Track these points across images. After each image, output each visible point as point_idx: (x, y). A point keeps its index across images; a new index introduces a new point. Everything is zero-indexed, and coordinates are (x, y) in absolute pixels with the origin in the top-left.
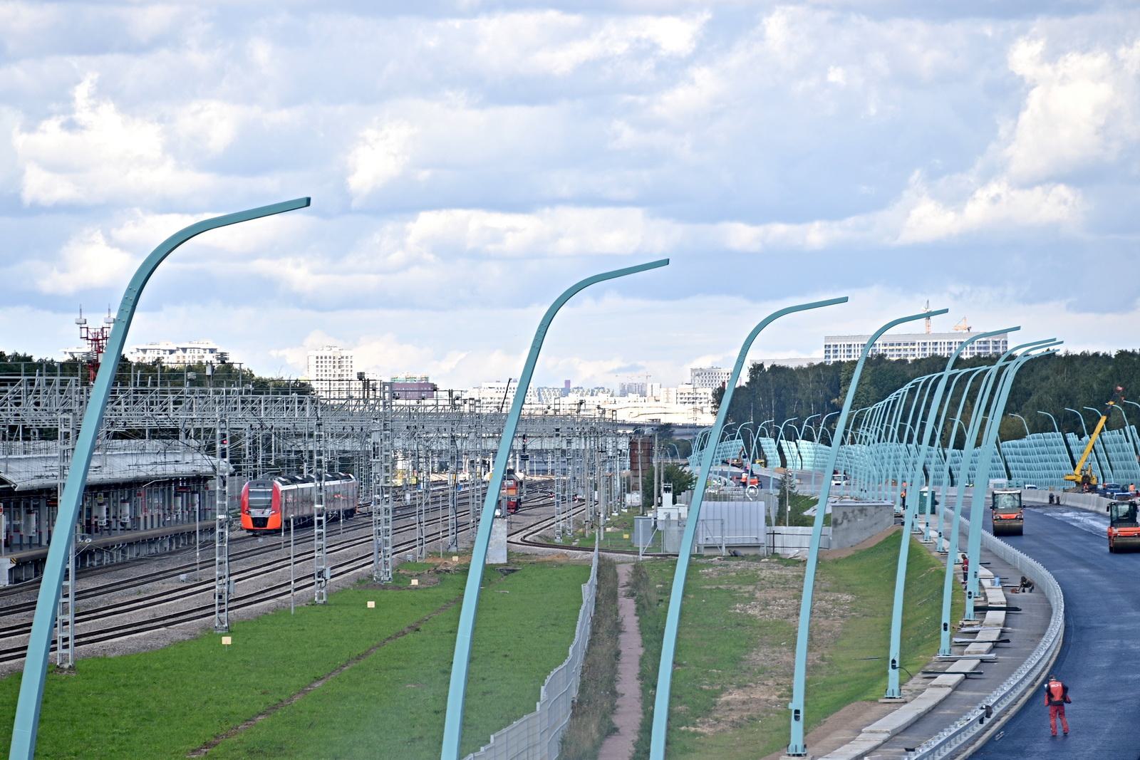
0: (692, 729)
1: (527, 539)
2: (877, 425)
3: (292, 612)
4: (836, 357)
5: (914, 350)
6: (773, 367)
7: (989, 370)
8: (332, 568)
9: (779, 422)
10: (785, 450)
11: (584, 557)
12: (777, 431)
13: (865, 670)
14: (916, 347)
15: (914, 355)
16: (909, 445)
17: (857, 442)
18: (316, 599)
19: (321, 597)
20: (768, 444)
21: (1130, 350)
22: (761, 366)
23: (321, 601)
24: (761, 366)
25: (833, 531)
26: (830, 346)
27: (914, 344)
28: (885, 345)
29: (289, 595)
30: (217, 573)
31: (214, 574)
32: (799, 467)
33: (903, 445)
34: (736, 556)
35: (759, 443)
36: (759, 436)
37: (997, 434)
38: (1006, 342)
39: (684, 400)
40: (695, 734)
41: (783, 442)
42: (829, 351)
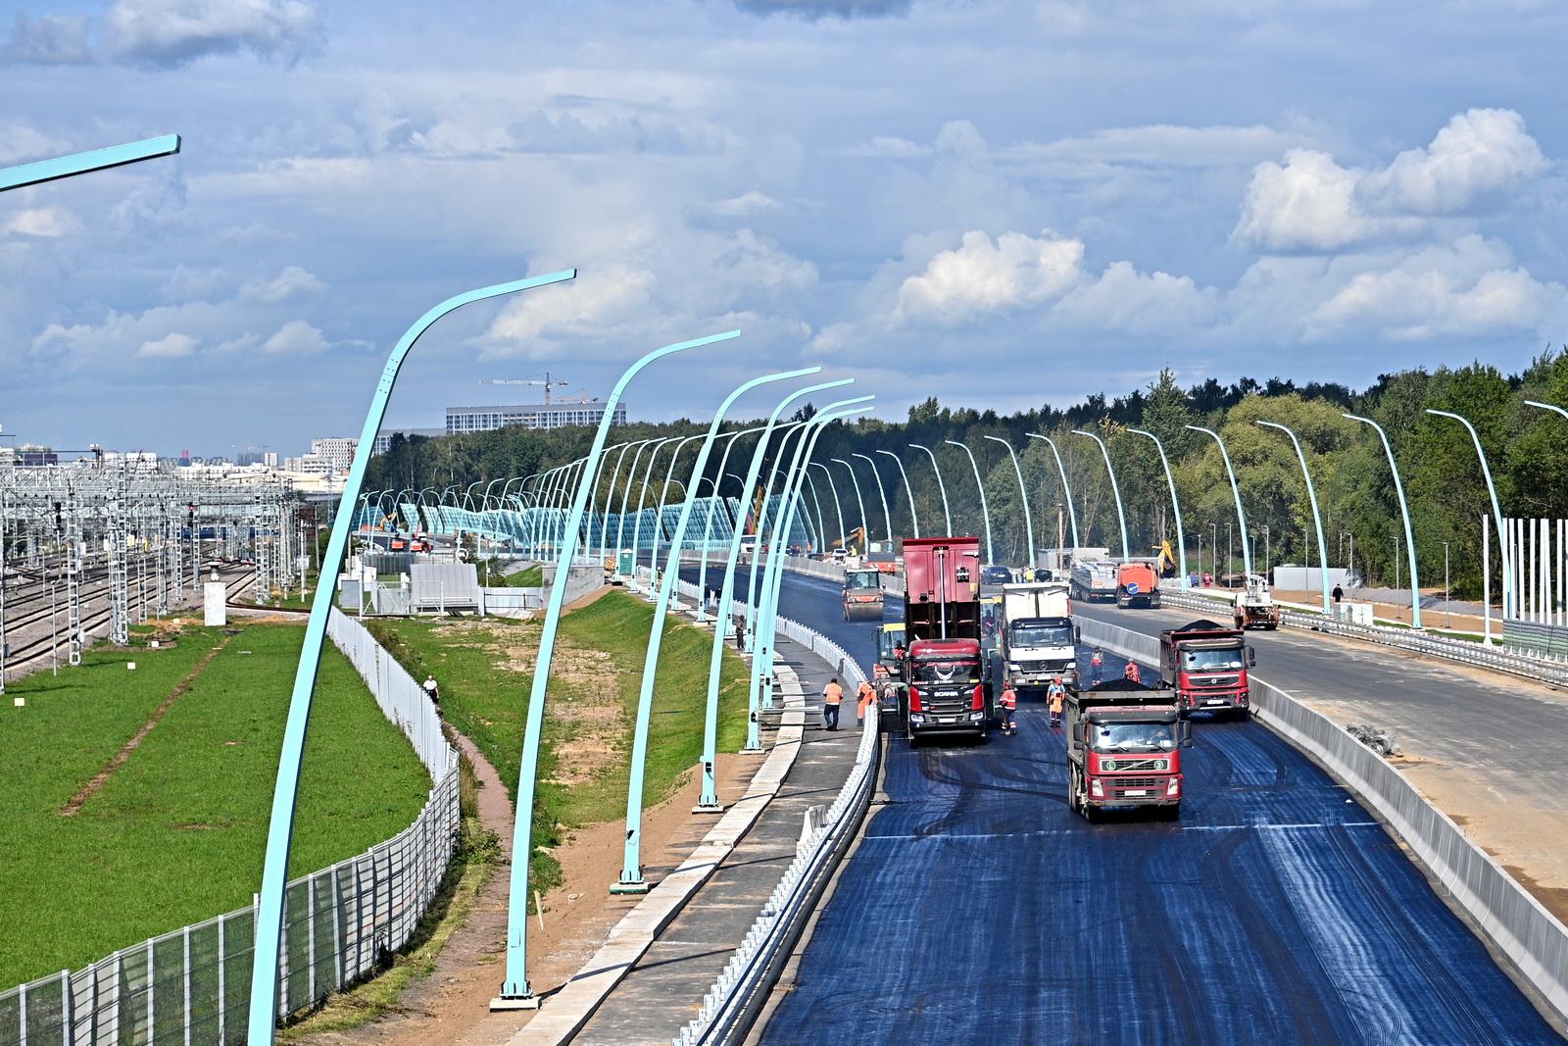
0: (553, 782)
1: (231, 600)
2: (561, 486)
3: (55, 674)
4: (458, 427)
5: (534, 420)
6: (412, 436)
7: (805, 426)
8: (86, 631)
9: (417, 489)
10: (427, 515)
11: (301, 618)
12: (417, 496)
13: (678, 724)
14: (537, 417)
15: (534, 425)
16: (564, 510)
17: (501, 506)
18: (71, 661)
19: (75, 658)
20: (409, 509)
21: (1025, 412)
22: (401, 435)
23: (76, 663)
24: (401, 435)
25: (545, 592)
26: (451, 417)
27: (534, 415)
28: (506, 416)
29: (52, 652)
30: (70, 619)
31: (66, 620)
32: (441, 532)
33: (558, 510)
34: (455, 616)
35: (399, 508)
36: (399, 502)
37: (745, 488)
38: (625, 413)
39: (308, 469)
40: (558, 786)
41: (424, 507)
42: (451, 422)
